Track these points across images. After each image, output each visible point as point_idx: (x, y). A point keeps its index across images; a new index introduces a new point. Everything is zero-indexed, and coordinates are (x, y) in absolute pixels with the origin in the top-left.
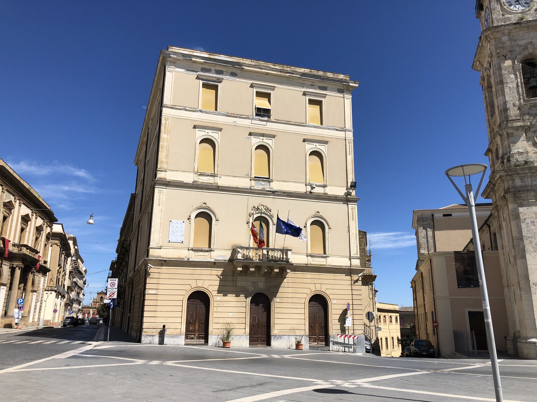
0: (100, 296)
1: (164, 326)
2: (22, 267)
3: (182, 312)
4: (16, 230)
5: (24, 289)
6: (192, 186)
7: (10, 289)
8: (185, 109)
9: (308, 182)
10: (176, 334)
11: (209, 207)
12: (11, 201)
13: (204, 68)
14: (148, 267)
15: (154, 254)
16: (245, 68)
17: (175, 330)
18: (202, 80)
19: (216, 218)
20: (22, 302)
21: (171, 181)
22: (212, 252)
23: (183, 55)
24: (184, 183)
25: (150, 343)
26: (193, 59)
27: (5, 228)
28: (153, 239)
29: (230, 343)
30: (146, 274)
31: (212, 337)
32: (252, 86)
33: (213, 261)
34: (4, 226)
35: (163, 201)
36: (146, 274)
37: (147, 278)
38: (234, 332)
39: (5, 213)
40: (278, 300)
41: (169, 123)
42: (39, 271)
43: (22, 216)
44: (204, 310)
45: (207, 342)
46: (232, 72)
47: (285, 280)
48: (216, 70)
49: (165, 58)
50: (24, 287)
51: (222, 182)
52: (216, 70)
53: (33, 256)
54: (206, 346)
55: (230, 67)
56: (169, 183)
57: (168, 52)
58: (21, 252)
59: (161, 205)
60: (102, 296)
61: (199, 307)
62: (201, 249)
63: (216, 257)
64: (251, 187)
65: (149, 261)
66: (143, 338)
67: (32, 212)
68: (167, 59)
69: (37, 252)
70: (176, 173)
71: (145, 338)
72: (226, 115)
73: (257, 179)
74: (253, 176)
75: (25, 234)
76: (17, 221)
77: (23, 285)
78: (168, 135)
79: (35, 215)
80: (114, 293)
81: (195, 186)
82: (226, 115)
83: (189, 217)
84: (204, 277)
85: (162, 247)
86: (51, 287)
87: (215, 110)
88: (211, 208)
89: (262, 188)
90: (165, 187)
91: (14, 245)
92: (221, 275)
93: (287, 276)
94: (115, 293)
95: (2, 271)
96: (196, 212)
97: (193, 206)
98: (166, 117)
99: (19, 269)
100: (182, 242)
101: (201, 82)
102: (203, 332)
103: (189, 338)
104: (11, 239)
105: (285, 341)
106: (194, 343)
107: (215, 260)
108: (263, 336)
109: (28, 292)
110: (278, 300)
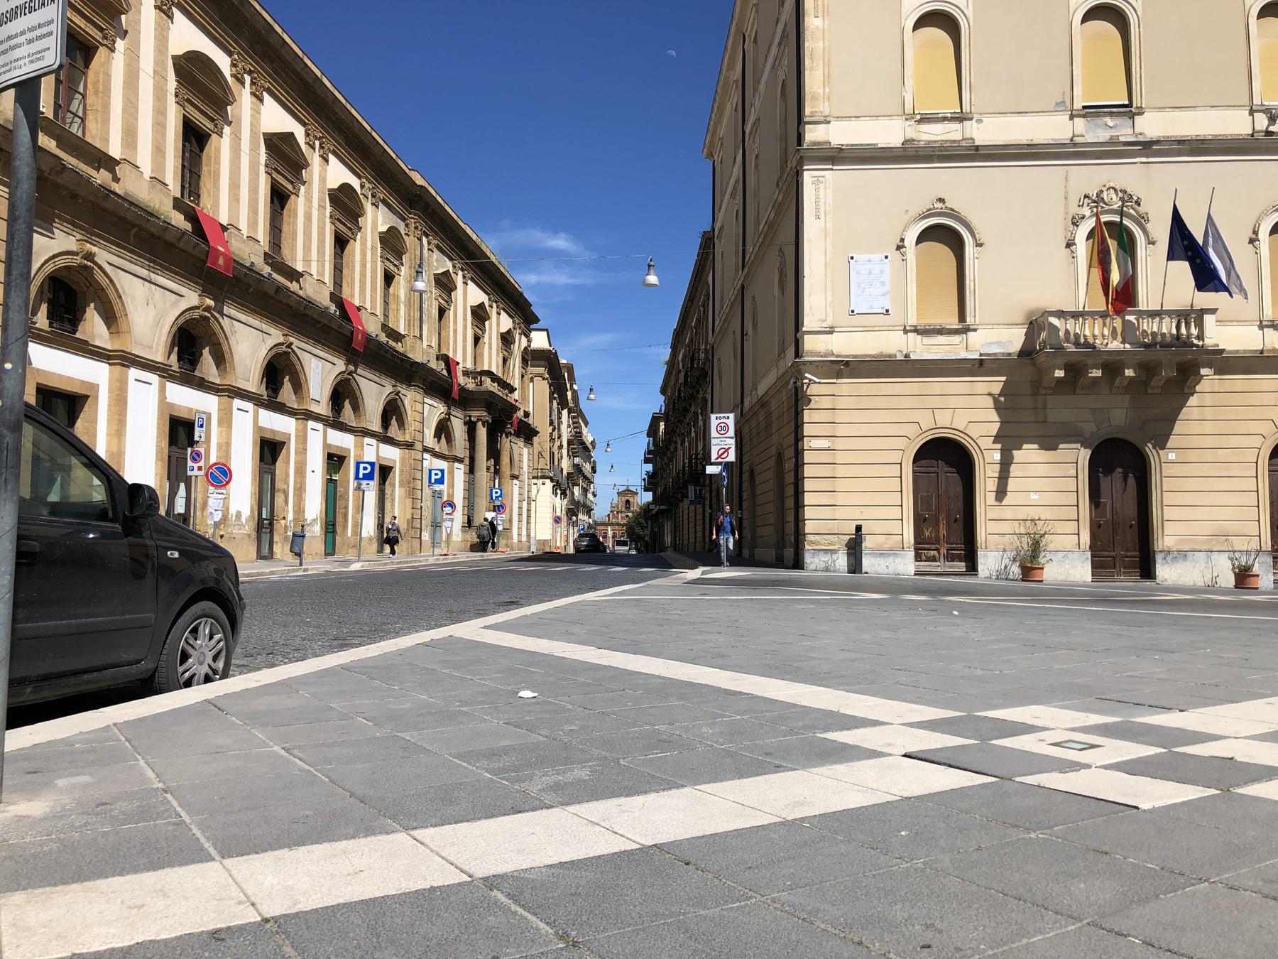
0: (624, 499)
1: (859, 528)
2: (487, 421)
3: (901, 492)
4: (465, 340)
5: (497, 472)
6: (902, 154)
7: (471, 470)
9: (1256, 101)
11: (952, 210)
14: (805, 381)
17: (887, 539)
20: (501, 496)
21: (844, 147)
22: (970, 334)
28: (811, 308)
29: (1043, 568)
30: (797, 400)
31: (986, 556)
33: (976, 356)
34: (442, 331)
36: (798, 400)
38: (1052, 542)
39: (440, 299)
40: (1172, 456)
42: (518, 434)
43: (471, 306)
45: (972, 567)
47: (1193, 401)
50: (495, 466)
51: (985, 132)
58: (482, 388)
59: (822, 216)
62: (938, 327)
63: (983, 345)
64: (1075, 139)
65: (804, 367)
66: (808, 559)
67: (490, 300)
70: (854, 123)
73: (1091, 112)
74: (1078, 105)
76: (465, 319)
79: (494, 305)
80: (727, 450)
81: (910, 154)
84: (953, 401)
85: (836, 330)
86: (542, 469)
89: (1108, 137)
91: (466, 373)
92: (1000, 395)
93: (1198, 388)
94: (729, 448)
96: (917, 227)
97: (907, 211)
99: (484, 427)
100: (887, 311)
102: (960, 544)
103: (923, 558)
104: (459, 359)
105: (1198, 565)
106: (939, 570)
107: (981, 355)
108: (1129, 554)
110: (1172, 456)
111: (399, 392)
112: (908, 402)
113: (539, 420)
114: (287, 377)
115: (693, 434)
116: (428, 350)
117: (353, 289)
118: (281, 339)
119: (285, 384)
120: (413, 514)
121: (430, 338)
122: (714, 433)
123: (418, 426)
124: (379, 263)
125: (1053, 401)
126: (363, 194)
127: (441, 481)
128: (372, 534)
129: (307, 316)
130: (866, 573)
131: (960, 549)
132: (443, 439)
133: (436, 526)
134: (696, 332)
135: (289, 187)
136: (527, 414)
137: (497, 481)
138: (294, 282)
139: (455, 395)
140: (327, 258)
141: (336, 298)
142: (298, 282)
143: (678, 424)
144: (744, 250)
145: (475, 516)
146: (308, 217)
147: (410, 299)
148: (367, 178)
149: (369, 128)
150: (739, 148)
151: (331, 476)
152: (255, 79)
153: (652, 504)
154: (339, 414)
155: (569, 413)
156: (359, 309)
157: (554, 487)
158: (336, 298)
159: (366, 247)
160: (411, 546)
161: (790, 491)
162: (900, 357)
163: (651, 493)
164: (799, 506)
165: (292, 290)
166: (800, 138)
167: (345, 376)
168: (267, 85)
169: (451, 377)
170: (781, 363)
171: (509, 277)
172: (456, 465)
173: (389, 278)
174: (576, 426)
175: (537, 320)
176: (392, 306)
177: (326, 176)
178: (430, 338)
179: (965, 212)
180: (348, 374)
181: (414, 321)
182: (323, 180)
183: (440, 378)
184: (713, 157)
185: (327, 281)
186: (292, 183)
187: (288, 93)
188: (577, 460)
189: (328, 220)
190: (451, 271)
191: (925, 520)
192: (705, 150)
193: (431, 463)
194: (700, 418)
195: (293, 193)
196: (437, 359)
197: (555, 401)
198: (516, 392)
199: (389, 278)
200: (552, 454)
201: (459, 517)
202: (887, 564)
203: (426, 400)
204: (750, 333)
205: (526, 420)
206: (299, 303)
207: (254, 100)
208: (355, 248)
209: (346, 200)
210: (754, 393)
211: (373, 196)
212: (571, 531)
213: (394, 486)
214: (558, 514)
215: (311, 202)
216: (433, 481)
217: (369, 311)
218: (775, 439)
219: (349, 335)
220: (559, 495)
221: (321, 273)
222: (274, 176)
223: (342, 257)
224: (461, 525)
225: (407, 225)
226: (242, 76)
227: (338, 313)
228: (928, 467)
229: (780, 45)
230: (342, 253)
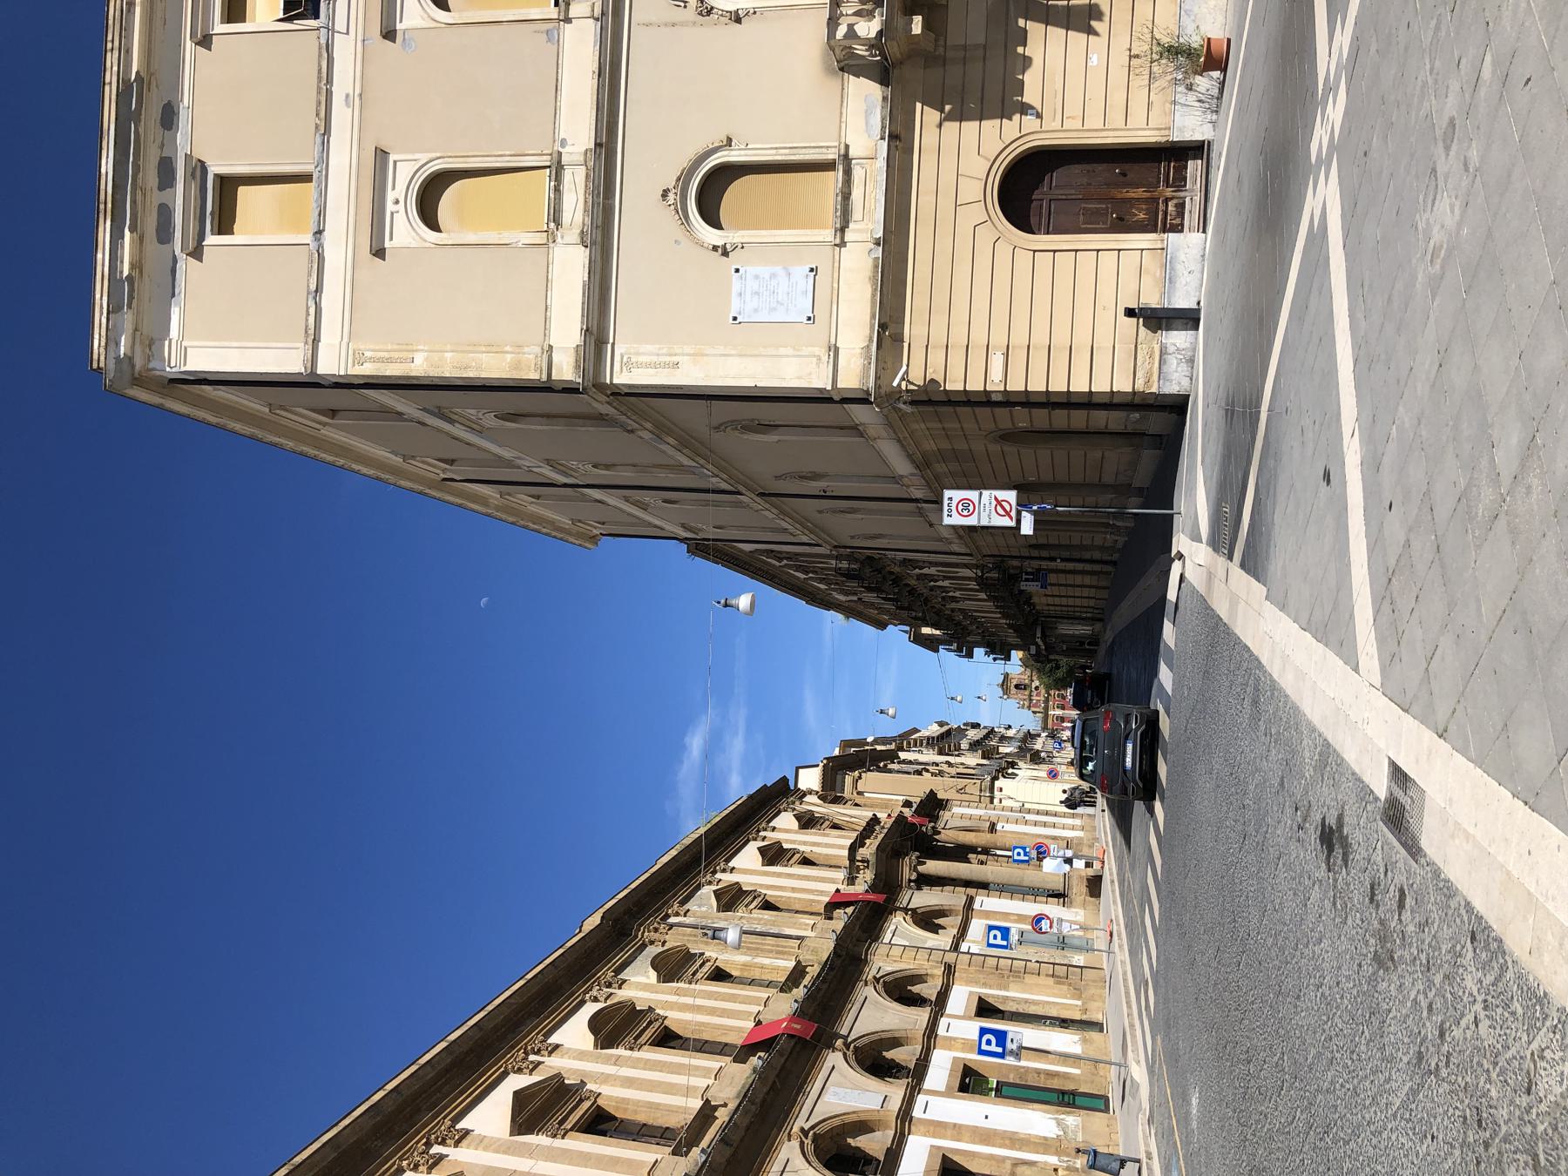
0: (1013, 690)
1: (1130, 313)
2: (918, 858)
4: (807, 878)
5: (986, 851)
7: (983, 886)
8: (316, 291)
10: (1161, 267)
12: (715, 892)
13: (157, 230)
15: (858, 371)
16: (135, 69)
18: (201, 236)
19: (721, 147)
21: (585, 327)
22: (852, 153)
23: (114, 309)
24: (589, 278)
25: (1191, 361)
26: (126, 273)
27: (797, 905)
28: (799, 378)
29: (1209, 39)
30: (930, 402)
31: (1180, 130)
32: (205, 41)
35: (661, 352)
37: (945, 389)
39: (752, 906)
41: (372, 347)
44: (1075, 172)
45: (1198, 149)
46: (158, 124)
48: (161, 188)
49: (136, 379)
51: (578, 134)
52: (161, 188)
53: (886, 831)
54: (1215, 147)
55: (141, 130)
56: (591, 333)
57: (112, 365)
58: (872, 860)
59: (675, 359)
60: (1012, 687)
61: (1062, 192)
62: (839, 198)
63: (869, 136)
66: (1172, 388)
67: (755, 839)
68: (138, 368)
69: (875, 821)
70: (554, 314)
71: (1172, 380)
72: (324, 134)
74: (553, 12)
75: (820, 854)
76: (779, 875)
77: (970, 856)
78: (417, 351)
79: (762, 834)
80: (999, 502)
82: (324, 134)
83: (717, 251)
84: (948, 177)
85: (833, 341)
86: (981, 790)
87: (311, 181)
88: (683, 171)
90: (609, 346)
91: (851, 880)
92: (942, 111)
94: (996, 499)
95: (928, 909)
98: (350, 361)
99: (924, 863)
100: (812, 270)
101: (211, 239)
103: (1178, 221)
104: (832, 888)
106: (1197, 199)
107: (882, 138)
109: (993, 841)
111: (875, 977)
112: (944, 243)
113: (917, 788)
114: (850, 1140)
115: (946, 583)
116: (818, 930)
117: (731, 1029)
118: (795, 1144)
119: (859, 1145)
120: (1047, 975)
121: (802, 926)
122: (972, 521)
123: (923, 955)
124: (698, 987)
125: (954, 37)
126: (606, 999)
127: (1005, 932)
128: (1076, 1038)
129: (764, 1101)
130: (1199, 303)
131: (1167, 168)
132: (940, 921)
133: (1063, 943)
134: (813, 572)
135: (586, 1105)
136: (907, 804)
137: (999, 852)
138: (716, 1114)
139: (880, 898)
140: (685, 1061)
141: (743, 1053)
142: (716, 1108)
143: (929, 605)
144: (714, 492)
145: (1049, 886)
146: (629, 1082)
147: (749, 948)
148: (585, 992)
149: (522, 982)
150: (583, 495)
151: (991, 1089)
152: (437, 1138)
153: (1029, 650)
154: (903, 1067)
155: (903, 750)
156: (759, 1023)
157: (1005, 777)
158: (743, 1053)
159: (676, 1003)
160: (1094, 981)
161: (1060, 419)
162: (879, 252)
163: (1012, 652)
164: (1088, 402)
165: (727, 1119)
166: (569, 390)
167: (849, 1053)
168: (448, 1122)
169: (856, 902)
170: (871, 432)
171: (727, 812)
172: (976, 906)
173: (719, 975)
174: (918, 743)
175: (784, 780)
176: (756, 974)
177: (576, 1050)
178: (802, 926)
179: (684, 162)
180: (848, 1050)
181: (778, 946)
182: (581, 1055)
183: (857, 918)
184: (597, 535)
185: (716, 1065)
186: (581, 1101)
187: (462, 1093)
188: (964, 745)
189: (636, 1054)
190: (715, 888)
191: (1120, 219)
192: (587, 545)
193: (974, 942)
194: (926, 571)
195: (595, 1101)
196: (831, 918)
197: (890, 766)
198: (879, 815)
199: (719, 975)
200: (960, 775)
201: (1052, 909)
202: (1186, 273)
203: (886, 940)
204: (822, 484)
205: (915, 806)
206: (746, 1112)
207: (465, 1143)
208: (677, 1019)
209: (610, 1026)
210: (905, 480)
211: (609, 985)
212: (1059, 760)
213: (1006, 998)
214: (1044, 774)
215: (609, 1076)
216: (1005, 943)
217: (761, 1008)
218: (978, 447)
219: (793, 1042)
220: (1015, 771)
221: (705, 1072)
222: (569, 1127)
223: (687, 1039)
224: (1061, 908)
225: (652, 943)
226: (432, 1156)
227: (762, 1054)
228: (1041, 213)
229: (452, 422)
230: (681, 1037)
